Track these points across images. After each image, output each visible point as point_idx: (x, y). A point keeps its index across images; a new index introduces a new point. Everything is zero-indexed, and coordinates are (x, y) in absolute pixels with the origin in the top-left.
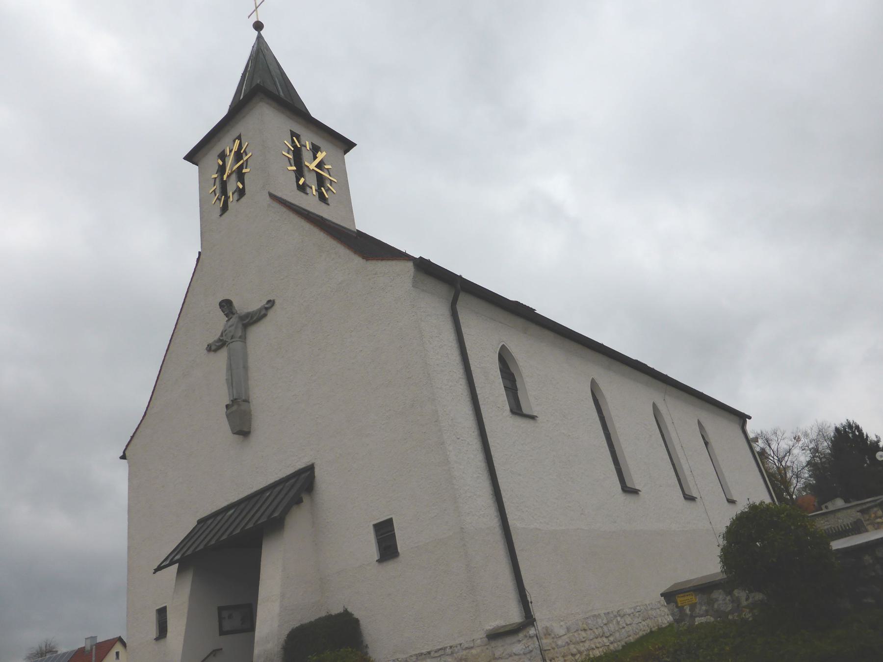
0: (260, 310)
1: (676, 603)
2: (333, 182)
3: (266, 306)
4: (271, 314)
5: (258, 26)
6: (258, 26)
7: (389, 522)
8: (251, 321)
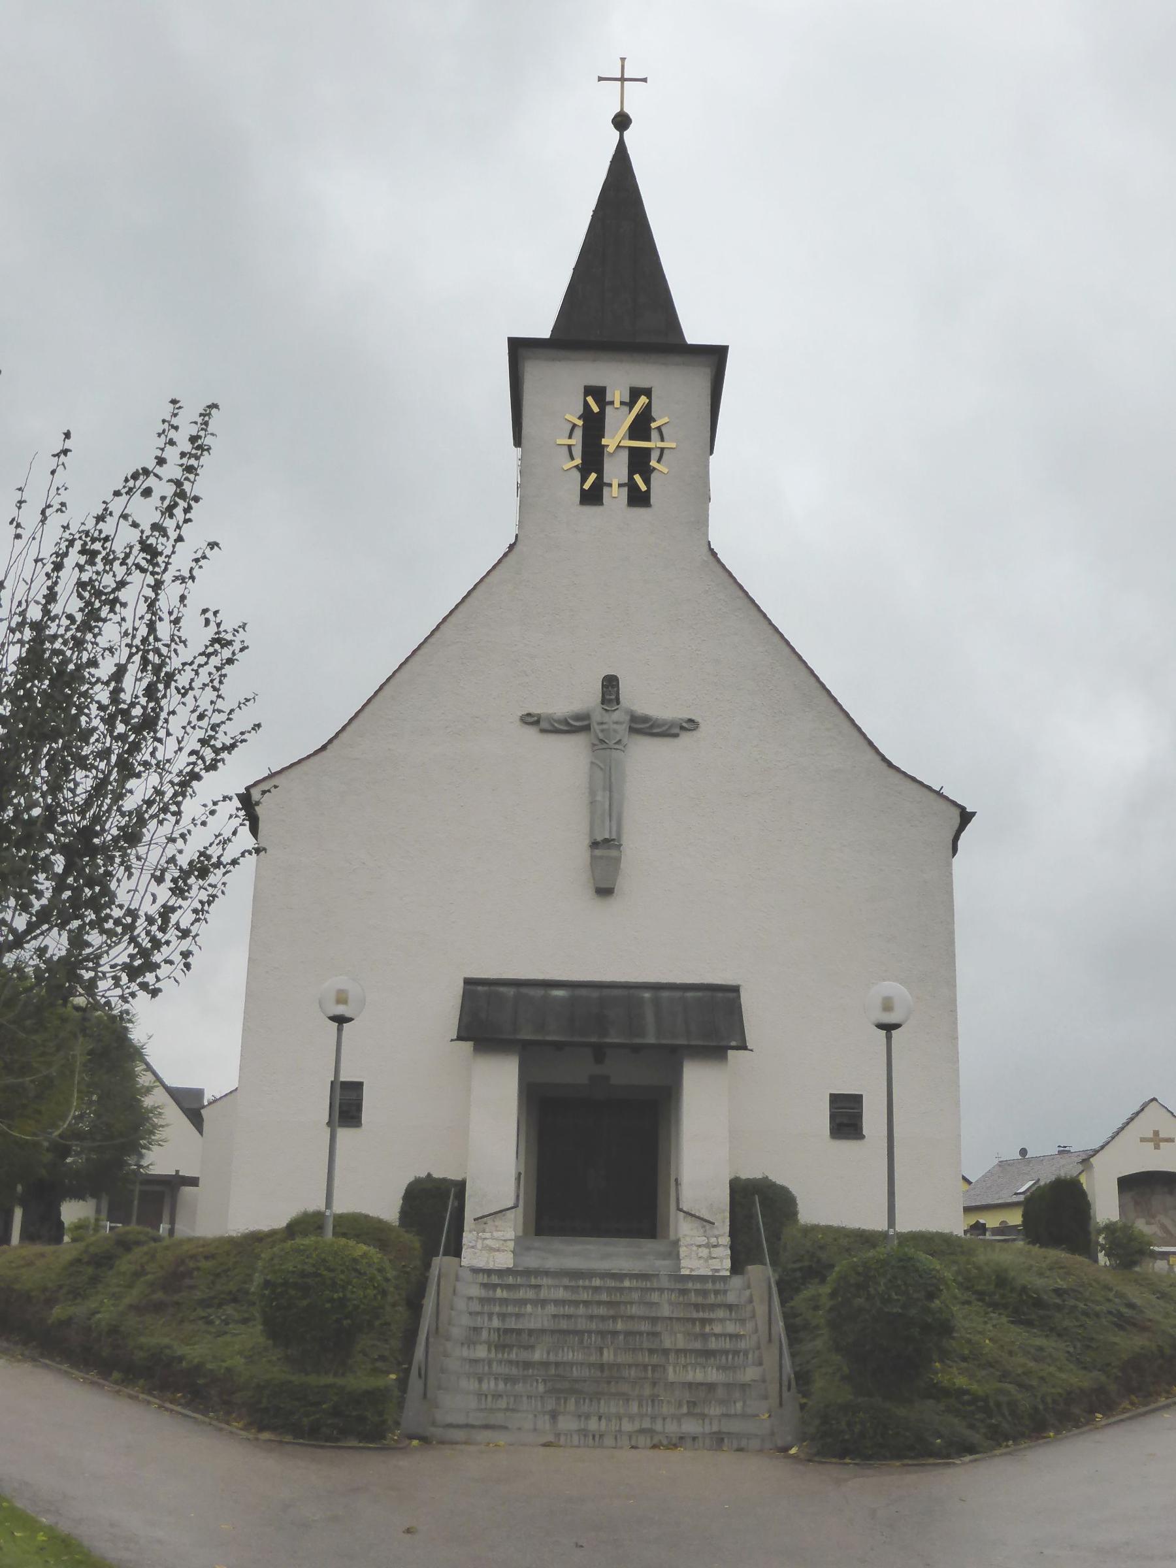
0: (672, 724)
1: (1169, 1261)
2: (620, 445)
3: (685, 725)
4: (685, 738)
5: (622, 122)
6: (622, 122)
7: (1141, 1138)
8: (648, 731)
